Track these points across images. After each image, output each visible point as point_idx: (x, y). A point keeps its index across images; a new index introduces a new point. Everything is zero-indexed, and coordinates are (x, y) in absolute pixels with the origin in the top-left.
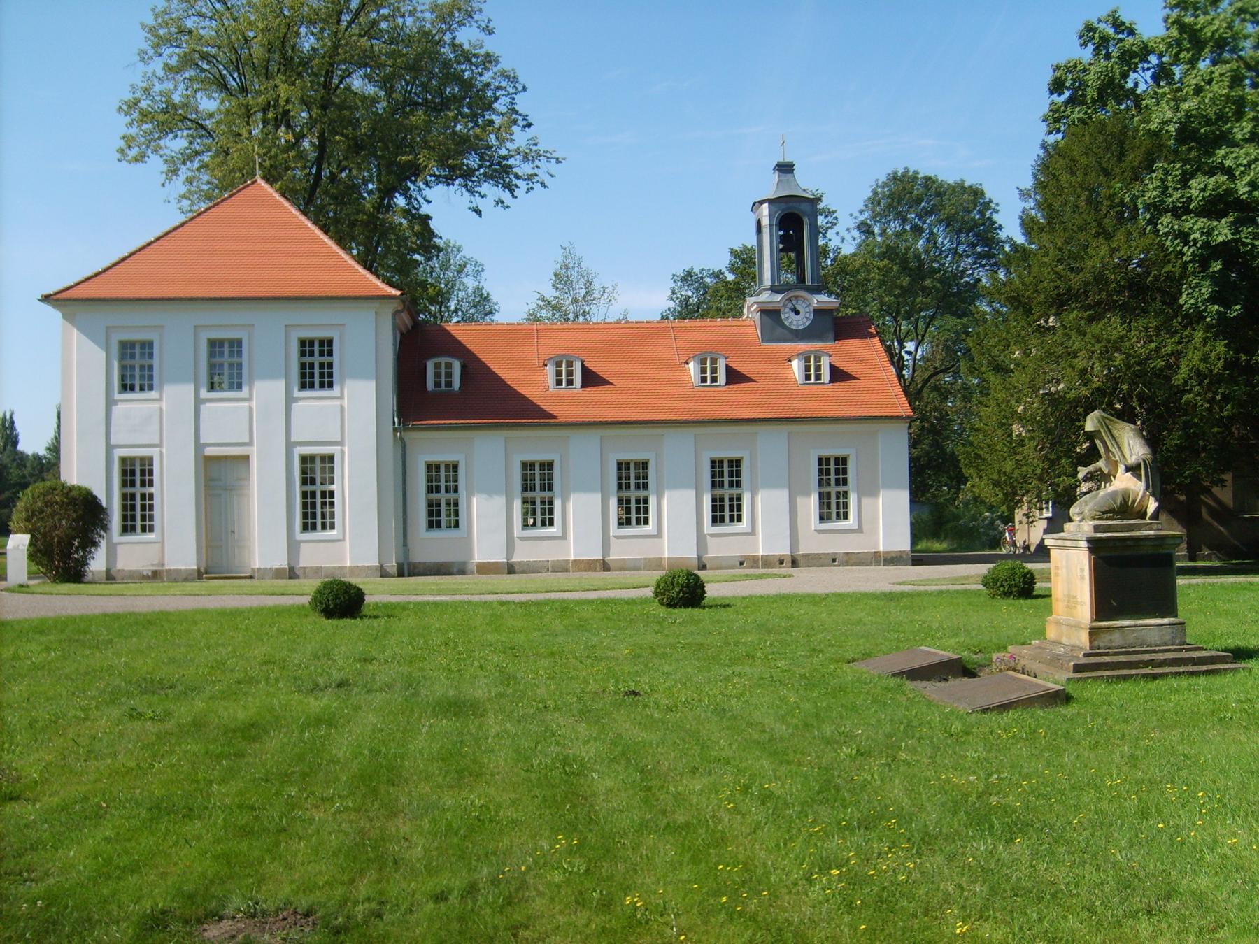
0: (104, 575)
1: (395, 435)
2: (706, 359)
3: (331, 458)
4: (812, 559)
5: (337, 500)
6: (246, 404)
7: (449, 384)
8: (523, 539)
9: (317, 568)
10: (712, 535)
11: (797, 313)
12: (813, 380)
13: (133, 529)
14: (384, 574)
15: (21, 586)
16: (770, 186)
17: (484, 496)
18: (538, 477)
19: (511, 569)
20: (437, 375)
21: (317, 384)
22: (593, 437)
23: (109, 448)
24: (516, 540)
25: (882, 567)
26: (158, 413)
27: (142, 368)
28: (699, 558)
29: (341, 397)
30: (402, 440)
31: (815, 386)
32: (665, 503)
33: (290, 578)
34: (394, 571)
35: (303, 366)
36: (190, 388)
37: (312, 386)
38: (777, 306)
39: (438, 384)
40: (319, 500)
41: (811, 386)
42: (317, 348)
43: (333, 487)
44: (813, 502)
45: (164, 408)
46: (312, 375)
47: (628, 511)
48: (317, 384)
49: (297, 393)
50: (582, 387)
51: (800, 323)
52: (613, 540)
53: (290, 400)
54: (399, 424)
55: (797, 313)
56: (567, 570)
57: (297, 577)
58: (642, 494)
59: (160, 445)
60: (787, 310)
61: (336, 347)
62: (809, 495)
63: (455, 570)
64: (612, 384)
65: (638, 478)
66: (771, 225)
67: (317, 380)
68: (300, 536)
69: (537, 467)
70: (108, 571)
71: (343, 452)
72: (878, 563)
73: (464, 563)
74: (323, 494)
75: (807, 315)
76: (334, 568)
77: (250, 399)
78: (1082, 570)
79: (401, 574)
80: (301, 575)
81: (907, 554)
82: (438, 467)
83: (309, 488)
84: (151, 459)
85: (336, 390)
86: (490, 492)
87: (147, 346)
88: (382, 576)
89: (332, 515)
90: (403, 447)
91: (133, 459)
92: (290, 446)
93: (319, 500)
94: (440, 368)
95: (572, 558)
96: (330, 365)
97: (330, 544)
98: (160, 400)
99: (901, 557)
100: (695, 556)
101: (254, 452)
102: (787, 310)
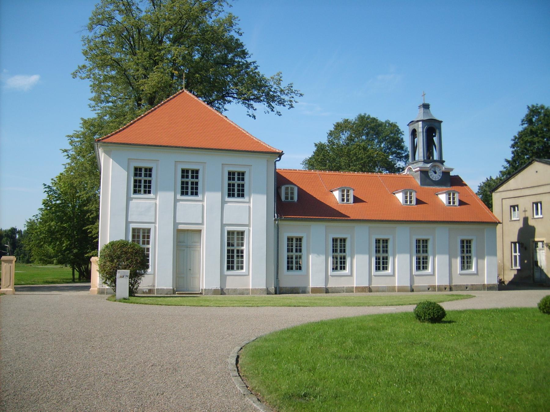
0: (409, 289)
1: (275, 223)
2: (344, 190)
3: (242, 233)
4: (458, 287)
6: (201, 203)
7: (292, 198)
8: (332, 276)
9: (235, 289)
10: (416, 275)
11: (435, 173)
12: (345, 201)
14: (269, 293)
15: (125, 299)
16: (420, 115)
17: (316, 255)
18: (339, 246)
19: (327, 291)
20: (287, 194)
21: (189, 193)
23: (127, 223)
24: (329, 276)
25: (486, 291)
26: (154, 206)
27: (145, 182)
28: (411, 286)
29: (249, 202)
30: (278, 225)
31: (409, 206)
32: (355, 261)
33: (326, 293)
34: (273, 291)
39: (287, 198)
40: (235, 254)
41: (345, 204)
43: (242, 248)
44: (459, 260)
45: (158, 203)
46: (234, 190)
49: (227, 199)
50: (353, 203)
51: (437, 178)
52: (373, 277)
53: (223, 202)
54: (278, 217)
55: (435, 173)
56: (353, 292)
57: (224, 294)
58: (385, 255)
59: (155, 223)
60: (431, 171)
61: (154, 173)
63: (301, 291)
64: (468, 204)
65: (383, 247)
66: (423, 132)
67: (236, 193)
68: (227, 273)
70: (222, 290)
71: (249, 230)
72: (484, 289)
73: (306, 288)
74: (238, 251)
76: (243, 289)
77: (202, 201)
81: (496, 285)
82: (292, 239)
83: (231, 248)
85: (200, 197)
86: (318, 253)
87: (195, 173)
88: (267, 294)
89: (242, 262)
90: (278, 228)
91: (139, 229)
92: (223, 226)
93: (235, 254)
95: (355, 286)
96: (197, 183)
97: (242, 277)
98: (155, 199)
99: (494, 287)
100: (172, 288)
101: (204, 228)
102: (431, 171)
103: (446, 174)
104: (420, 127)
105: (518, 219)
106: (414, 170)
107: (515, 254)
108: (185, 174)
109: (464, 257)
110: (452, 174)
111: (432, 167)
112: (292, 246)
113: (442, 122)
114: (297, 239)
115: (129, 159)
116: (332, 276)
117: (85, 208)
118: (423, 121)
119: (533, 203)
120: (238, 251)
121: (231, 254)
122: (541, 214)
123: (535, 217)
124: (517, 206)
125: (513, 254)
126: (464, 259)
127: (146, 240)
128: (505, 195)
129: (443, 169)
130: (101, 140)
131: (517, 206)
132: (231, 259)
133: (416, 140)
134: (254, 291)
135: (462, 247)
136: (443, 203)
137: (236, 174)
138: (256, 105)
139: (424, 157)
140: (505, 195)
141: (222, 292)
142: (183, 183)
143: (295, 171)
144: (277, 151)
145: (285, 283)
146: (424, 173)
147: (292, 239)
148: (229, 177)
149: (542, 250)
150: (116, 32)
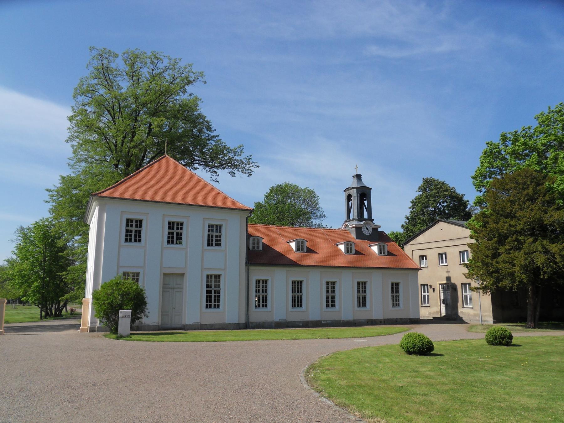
7: (258, 248)
11: (367, 229)
13: (295, 306)
16: (353, 183)
20: (254, 244)
21: (133, 240)
22: (317, 272)
35: (127, 231)
38: (361, 226)
39: (254, 247)
41: (300, 253)
42: (175, 226)
46: (131, 236)
59: (225, 269)
64: (316, 253)
67: (133, 238)
78: (389, 327)
82: (259, 282)
94: (299, 243)
102: (364, 228)
103: (375, 229)
104: (354, 193)
105: (426, 266)
106: (350, 227)
107: (424, 294)
108: (138, 224)
109: (393, 296)
110: (380, 230)
111: (364, 224)
113: (371, 189)
114: (263, 282)
115: (204, 218)
117: (60, 254)
118: (357, 188)
119: (439, 254)
121: (209, 294)
122: (446, 262)
123: (441, 264)
124: (426, 256)
125: (423, 294)
126: (393, 298)
128: (415, 247)
129: (373, 226)
130: (96, 194)
131: (426, 256)
132: (209, 299)
133: (350, 203)
135: (359, 288)
136: (375, 253)
137: (134, 222)
138: (219, 171)
139: (358, 217)
140: (415, 247)
142: (169, 233)
143: (335, 231)
144: (249, 208)
146: (358, 230)
147: (259, 282)
148: (168, 227)
149: (448, 291)
150: (100, 104)
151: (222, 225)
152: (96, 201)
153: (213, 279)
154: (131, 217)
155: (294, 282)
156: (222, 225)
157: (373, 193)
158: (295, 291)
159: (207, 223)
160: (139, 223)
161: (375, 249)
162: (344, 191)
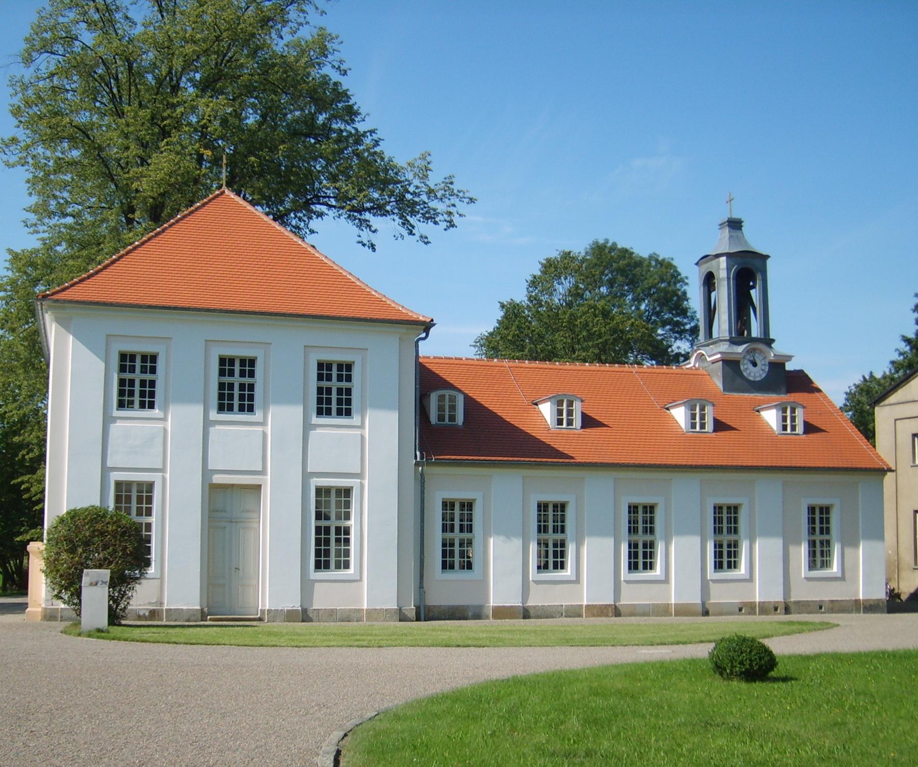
0: (700, 609)
1: (416, 471)
3: (347, 492)
5: (352, 537)
7: (452, 418)
8: (537, 582)
10: (714, 581)
11: (755, 364)
12: (565, 425)
14: (403, 618)
15: (99, 630)
16: (721, 242)
18: (551, 518)
19: (526, 614)
20: (441, 408)
21: (334, 411)
23: (105, 470)
28: (703, 604)
29: (362, 427)
30: (422, 475)
31: (699, 435)
33: (303, 621)
34: (412, 614)
36: (199, 409)
37: (230, 409)
39: (441, 418)
40: (333, 536)
41: (563, 431)
42: (237, 368)
43: (348, 523)
44: (804, 549)
45: (169, 429)
46: (231, 397)
47: (462, 554)
48: (334, 411)
49: (315, 420)
50: (582, 427)
51: (757, 375)
52: (623, 585)
53: (307, 427)
54: (422, 458)
55: (755, 364)
56: (580, 616)
57: (310, 620)
58: (648, 538)
59: (162, 470)
60: (746, 361)
61: (160, 365)
62: (799, 544)
65: (645, 522)
69: (551, 508)
70: (305, 611)
72: (858, 611)
73: (481, 607)
74: (338, 530)
75: (763, 367)
76: (350, 610)
77: (263, 424)
79: (418, 619)
80: (314, 618)
81: (883, 603)
82: (452, 505)
83: (323, 523)
84: (150, 486)
88: (400, 620)
89: (347, 553)
90: (422, 480)
91: (129, 484)
92: (306, 476)
93: (333, 536)
94: (786, 421)
95: (585, 603)
97: (347, 584)
98: (164, 419)
99: (878, 605)
100: (699, 601)
102: (746, 361)
103: (777, 366)
106: (709, 359)
109: (814, 542)
110: (789, 367)
111: (748, 351)
112: (452, 520)
114: (462, 505)
116: (537, 582)
118: (728, 255)
120: (338, 530)
126: (815, 546)
127: (144, 506)
129: (771, 356)
133: (713, 295)
134: (372, 614)
135: (812, 521)
136: (771, 428)
137: (335, 368)
141: (304, 616)
144: (421, 318)
145: (437, 598)
146: (731, 365)
147: (452, 505)
151: (354, 362)
152: (49, 312)
153: (333, 497)
154: (326, 357)
155: (633, 509)
156: (354, 362)
157: (771, 266)
158: (546, 530)
159: (315, 358)
160: (150, 361)
161: (771, 417)
162: (697, 264)
